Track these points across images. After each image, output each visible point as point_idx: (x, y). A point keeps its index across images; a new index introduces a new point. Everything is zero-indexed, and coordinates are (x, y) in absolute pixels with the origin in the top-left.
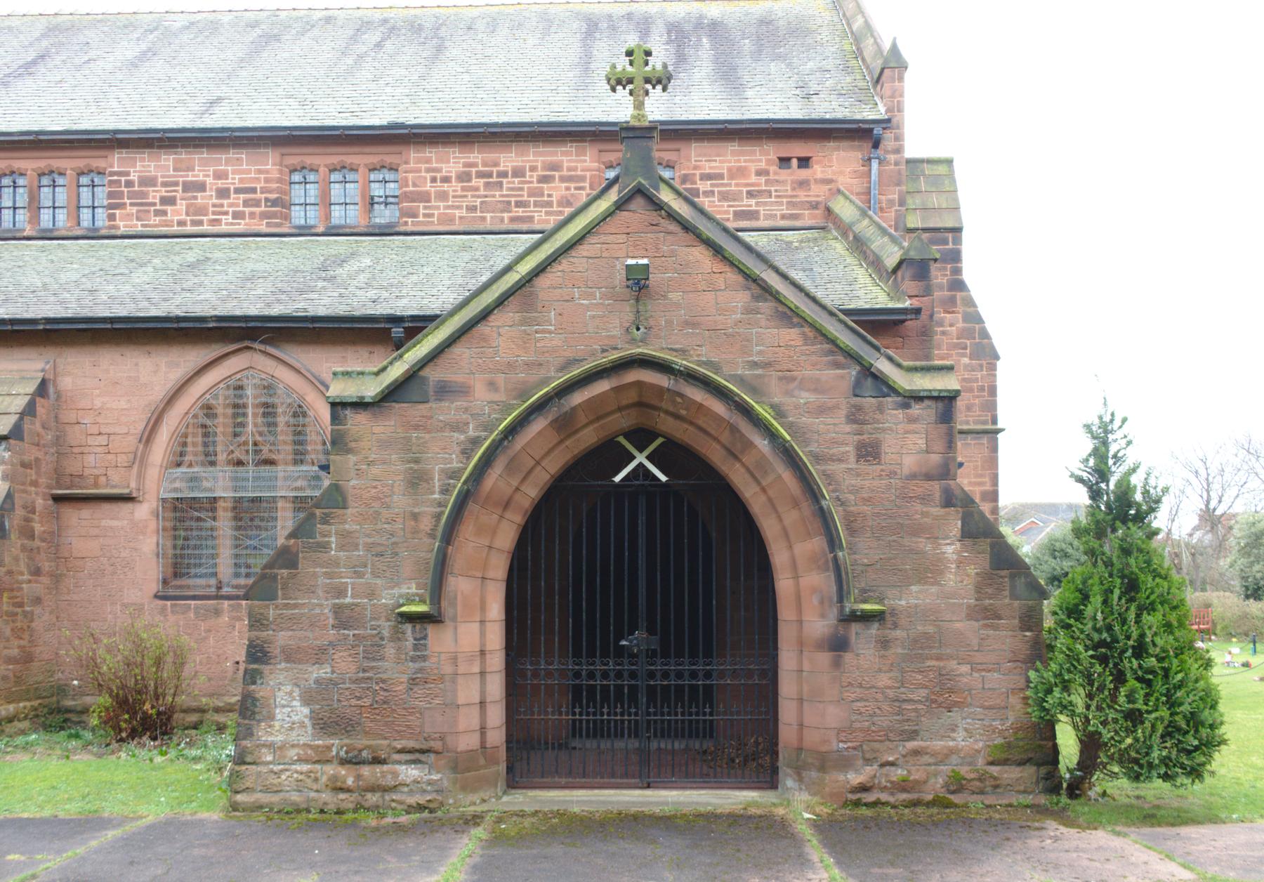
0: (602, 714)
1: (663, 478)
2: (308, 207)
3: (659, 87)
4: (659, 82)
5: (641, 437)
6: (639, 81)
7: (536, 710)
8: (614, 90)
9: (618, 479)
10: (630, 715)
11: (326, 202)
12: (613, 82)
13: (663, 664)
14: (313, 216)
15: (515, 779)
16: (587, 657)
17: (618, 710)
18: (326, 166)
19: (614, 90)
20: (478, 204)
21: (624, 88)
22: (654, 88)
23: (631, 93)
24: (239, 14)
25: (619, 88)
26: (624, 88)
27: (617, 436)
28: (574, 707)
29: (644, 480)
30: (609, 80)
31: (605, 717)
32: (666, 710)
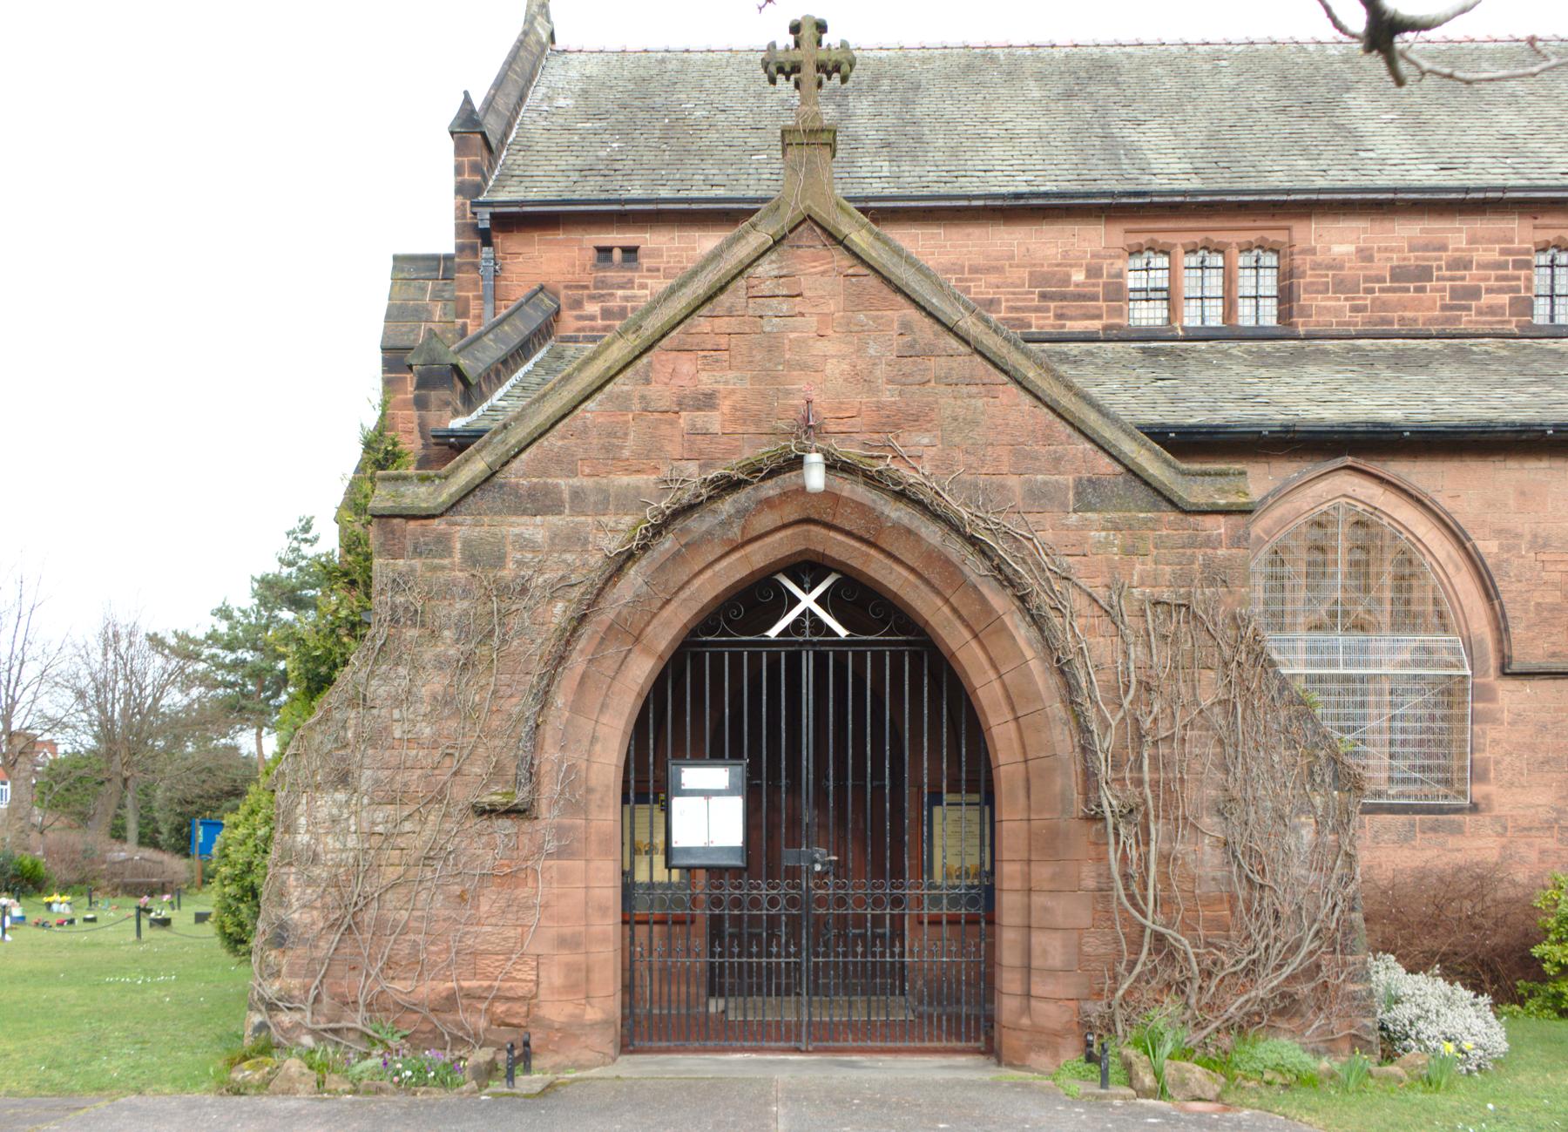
0: (855, 955)
1: (842, 632)
2: (1207, 302)
3: (836, 77)
4: (837, 68)
5: (807, 569)
6: (809, 72)
7: (860, 949)
8: (773, 81)
9: (773, 633)
10: (837, 955)
11: (1171, 297)
12: (773, 69)
13: (893, 887)
14: (1215, 319)
15: (627, 1045)
16: (891, 878)
17: (755, 949)
18: (1183, 245)
19: (773, 81)
20: (1368, 302)
21: (788, 79)
22: (829, 78)
23: (797, 86)
24: (1128, 49)
25: (781, 78)
26: (788, 79)
27: (777, 572)
28: (712, 945)
29: (813, 634)
30: (766, 67)
31: (859, 959)
32: (755, 949)
